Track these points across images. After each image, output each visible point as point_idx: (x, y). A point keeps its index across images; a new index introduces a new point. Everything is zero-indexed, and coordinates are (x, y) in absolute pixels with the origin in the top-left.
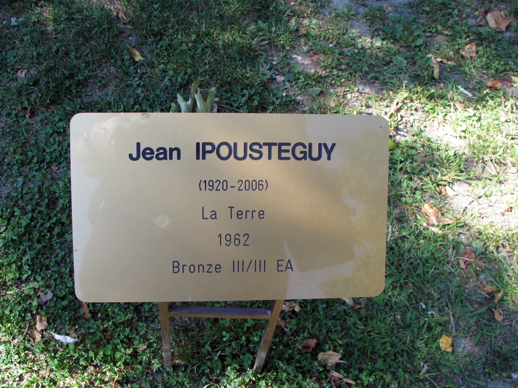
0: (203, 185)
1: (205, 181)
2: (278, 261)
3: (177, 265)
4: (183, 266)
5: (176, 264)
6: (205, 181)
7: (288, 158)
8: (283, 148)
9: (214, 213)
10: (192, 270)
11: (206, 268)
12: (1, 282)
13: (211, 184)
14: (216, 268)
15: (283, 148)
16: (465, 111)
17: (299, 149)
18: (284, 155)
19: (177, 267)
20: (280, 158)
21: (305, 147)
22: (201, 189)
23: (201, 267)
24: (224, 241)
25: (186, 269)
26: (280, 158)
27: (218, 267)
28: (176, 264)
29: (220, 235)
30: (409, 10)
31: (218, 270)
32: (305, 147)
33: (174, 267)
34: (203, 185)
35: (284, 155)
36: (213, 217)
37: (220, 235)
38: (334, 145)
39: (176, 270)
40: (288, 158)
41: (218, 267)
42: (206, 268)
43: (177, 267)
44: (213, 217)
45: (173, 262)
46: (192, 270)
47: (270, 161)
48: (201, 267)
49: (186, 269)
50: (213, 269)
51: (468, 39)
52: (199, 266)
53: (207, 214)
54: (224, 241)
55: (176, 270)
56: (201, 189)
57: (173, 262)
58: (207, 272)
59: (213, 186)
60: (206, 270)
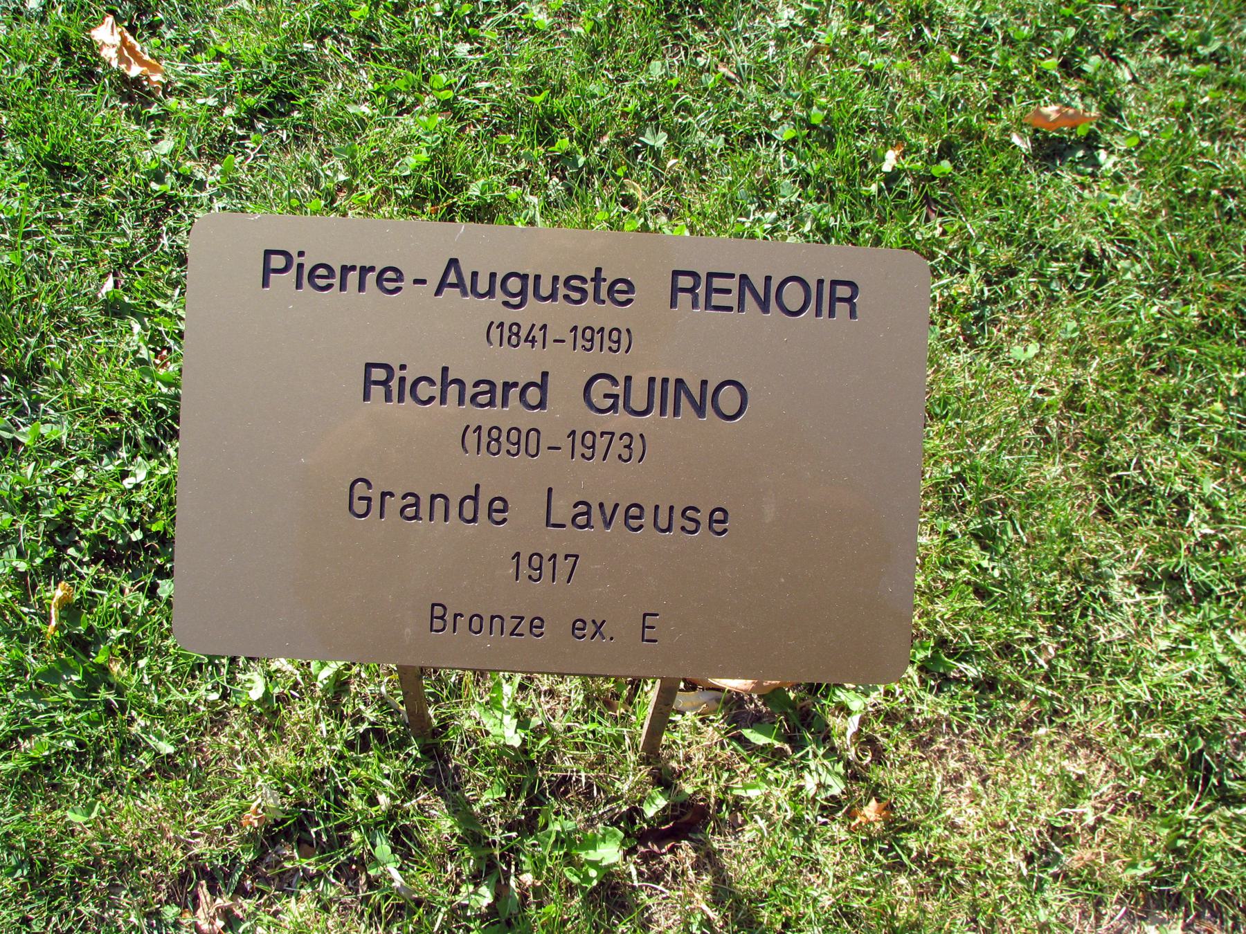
2: (645, 615)
3: (441, 614)
4: (456, 616)
7: (730, 309)
8: (718, 283)
10: (476, 626)
12: (1240, 29)
13: (589, 442)
15: (718, 283)
16: (875, 705)
17: (601, 386)
18: (717, 299)
19: (442, 618)
20: (708, 306)
21: (615, 382)
24: (525, 571)
26: (708, 306)
27: (537, 624)
28: (438, 611)
30: (1197, 718)
32: (615, 382)
33: (432, 617)
35: (717, 299)
37: (518, 554)
40: (730, 309)
42: (509, 624)
43: (442, 618)
45: (433, 605)
46: (476, 626)
54: (525, 571)
55: (438, 624)
57: (433, 605)
58: (512, 634)
59: (593, 447)
60: (507, 630)
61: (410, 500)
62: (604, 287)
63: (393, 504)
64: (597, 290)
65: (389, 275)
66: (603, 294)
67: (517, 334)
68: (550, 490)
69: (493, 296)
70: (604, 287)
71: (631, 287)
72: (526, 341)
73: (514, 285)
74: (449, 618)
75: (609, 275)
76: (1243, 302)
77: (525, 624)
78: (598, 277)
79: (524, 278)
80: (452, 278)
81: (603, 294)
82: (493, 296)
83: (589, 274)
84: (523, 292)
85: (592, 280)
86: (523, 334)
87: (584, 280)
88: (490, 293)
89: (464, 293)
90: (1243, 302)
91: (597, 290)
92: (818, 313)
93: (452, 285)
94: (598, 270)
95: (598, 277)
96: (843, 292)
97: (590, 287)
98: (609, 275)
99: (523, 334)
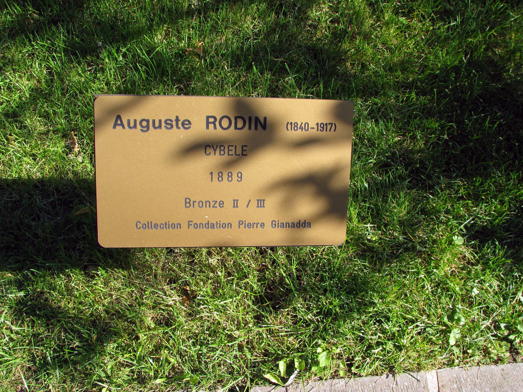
0: (289, 126)
1: (291, 123)
5: (188, 201)
11: (212, 204)
14: (220, 204)
23: (208, 203)
31: (221, 206)
33: (186, 203)
34: (289, 126)
39: (188, 205)
41: (221, 203)
46: (201, 205)
48: (208, 203)
49: (196, 204)
50: (217, 205)
52: (206, 202)
60: (211, 205)
62: (180, 123)
65: (186, 123)
71: (190, 123)
72: (300, 128)
73: (144, 124)
74: (191, 203)
75: (182, 119)
76: (435, 2)
77: (218, 203)
78: (177, 120)
79: (148, 121)
83: (174, 119)
84: (148, 127)
86: (299, 126)
87: (171, 121)
88: (135, 126)
89: (124, 127)
90: (435, 2)
93: (119, 125)
94: (177, 117)
95: (177, 120)
96: (211, 120)
97: (174, 123)
98: (182, 119)
99: (299, 126)
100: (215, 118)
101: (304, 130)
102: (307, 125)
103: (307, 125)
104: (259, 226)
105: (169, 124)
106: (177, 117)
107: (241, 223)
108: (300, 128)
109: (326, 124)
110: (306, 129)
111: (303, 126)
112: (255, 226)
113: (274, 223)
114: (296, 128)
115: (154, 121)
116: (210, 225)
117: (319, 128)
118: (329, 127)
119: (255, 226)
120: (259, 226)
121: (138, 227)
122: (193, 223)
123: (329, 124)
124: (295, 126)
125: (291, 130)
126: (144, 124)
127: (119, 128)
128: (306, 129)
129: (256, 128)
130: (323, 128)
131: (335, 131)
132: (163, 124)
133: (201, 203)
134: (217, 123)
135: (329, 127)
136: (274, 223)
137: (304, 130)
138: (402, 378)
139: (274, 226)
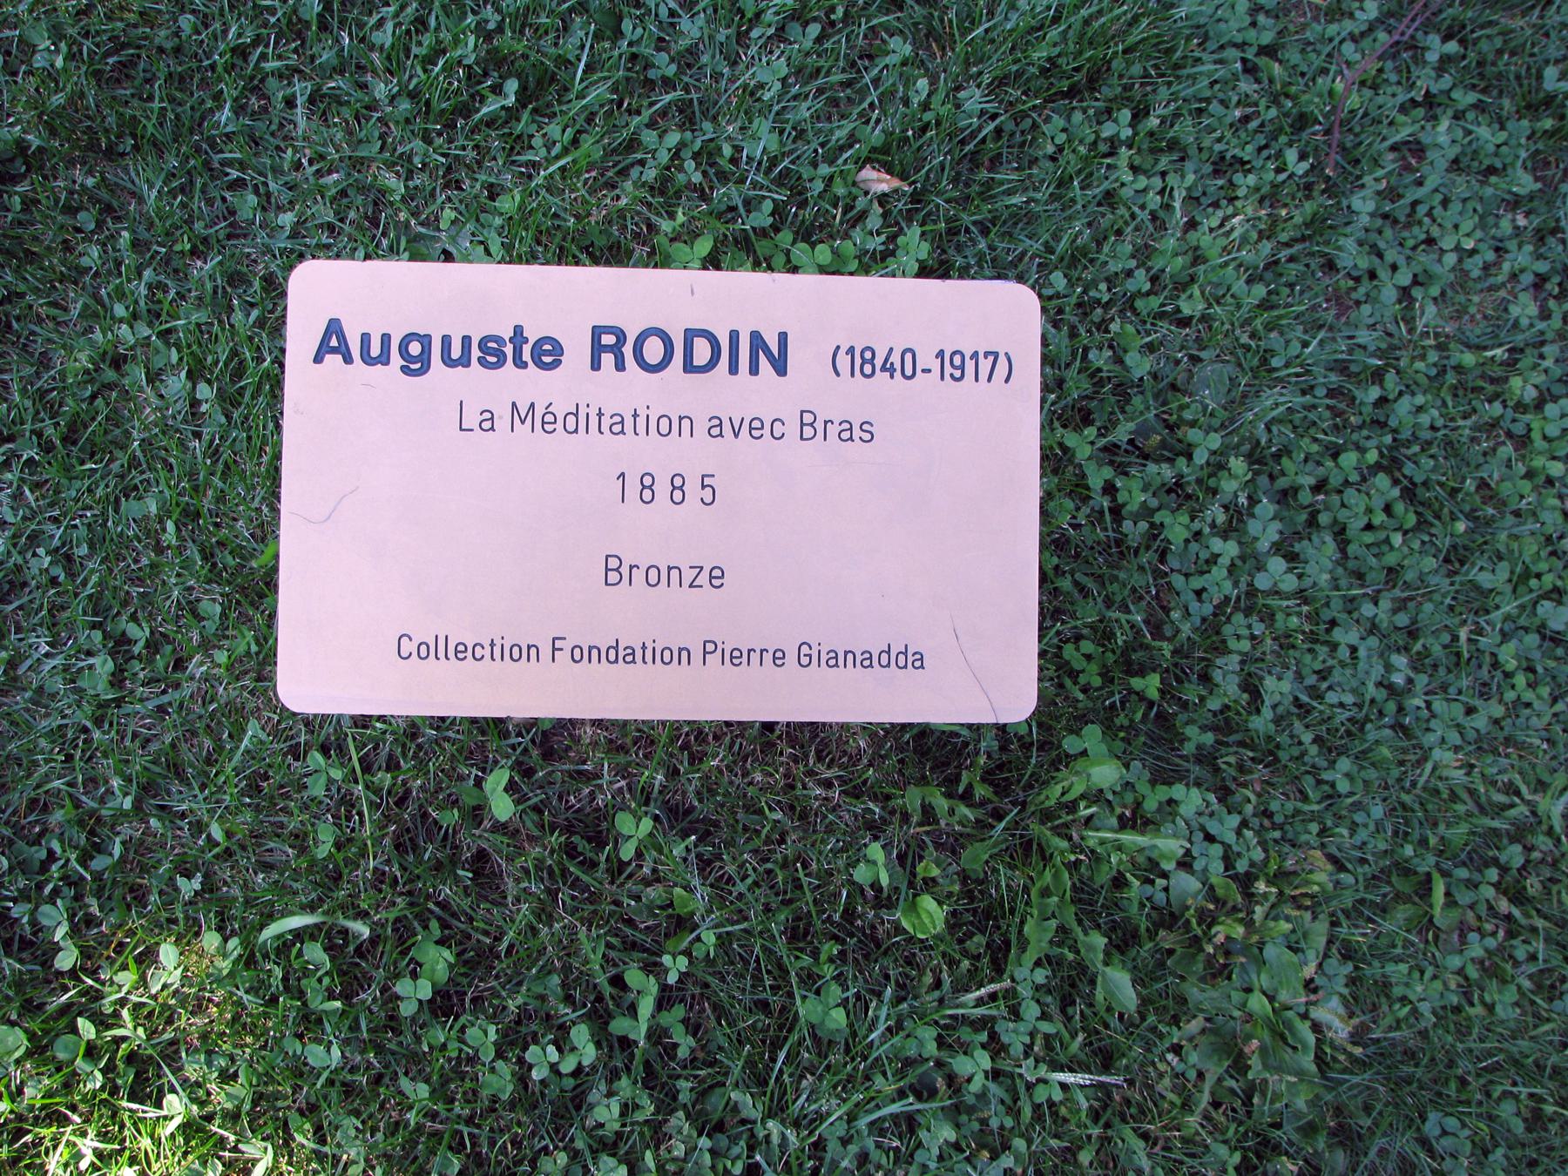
1: (851, 350)
4: (631, 567)
5: (613, 563)
6: (851, 350)
9: (488, 415)
11: (688, 575)
22: (838, 374)
23: (674, 573)
25: (638, 575)
28: (613, 563)
29: (623, 474)
31: (716, 582)
33: (607, 570)
36: (487, 425)
37: (623, 474)
38: (318, 359)
39: (614, 577)
42: (688, 575)
44: (487, 425)
46: (653, 580)
47: (1567, 599)
48: (674, 573)
49: (638, 575)
50: (704, 578)
51: (981, 136)
53: (472, 420)
56: (838, 374)
60: (686, 582)
61: (847, 426)
62: (527, 349)
63: (833, 430)
64: (518, 353)
66: (526, 356)
67: (872, 361)
68: (1007, 381)
69: (387, 363)
70: (527, 349)
72: (883, 369)
75: (532, 335)
77: (705, 575)
79: (425, 340)
80: (334, 343)
81: (526, 356)
82: (387, 363)
83: (507, 334)
85: (511, 340)
86: (879, 362)
89: (348, 359)
91: (518, 353)
92: (733, 369)
93: (334, 351)
96: (608, 340)
98: (532, 335)
99: (879, 362)
100: (621, 336)
101: (898, 374)
102: (908, 357)
103: (908, 357)
104: (768, 657)
105: (492, 353)
106: (518, 330)
107: (710, 647)
108: (883, 369)
109: (975, 355)
110: (909, 372)
111: (895, 359)
112: (755, 657)
113: (805, 649)
114: (868, 369)
115: (446, 341)
116: (621, 654)
117: (948, 369)
118: (985, 365)
119: (755, 657)
120: (768, 657)
121: (404, 654)
122: (566, 645)
123: (986, 354)
124: (864, 361)
125: (853, 375)
126: (415, 348)
127: (334, 360)
128: (909, 372)
129: (754, 370)
130: (962, 368)
131: (989, 380)
132: (476, 353)
133: (653, 572)
134: (628, 350)
135: (985, 365)
136: (805, 649)
137: (898, 374)
138: (1563, 223)
139: (805, 661)
